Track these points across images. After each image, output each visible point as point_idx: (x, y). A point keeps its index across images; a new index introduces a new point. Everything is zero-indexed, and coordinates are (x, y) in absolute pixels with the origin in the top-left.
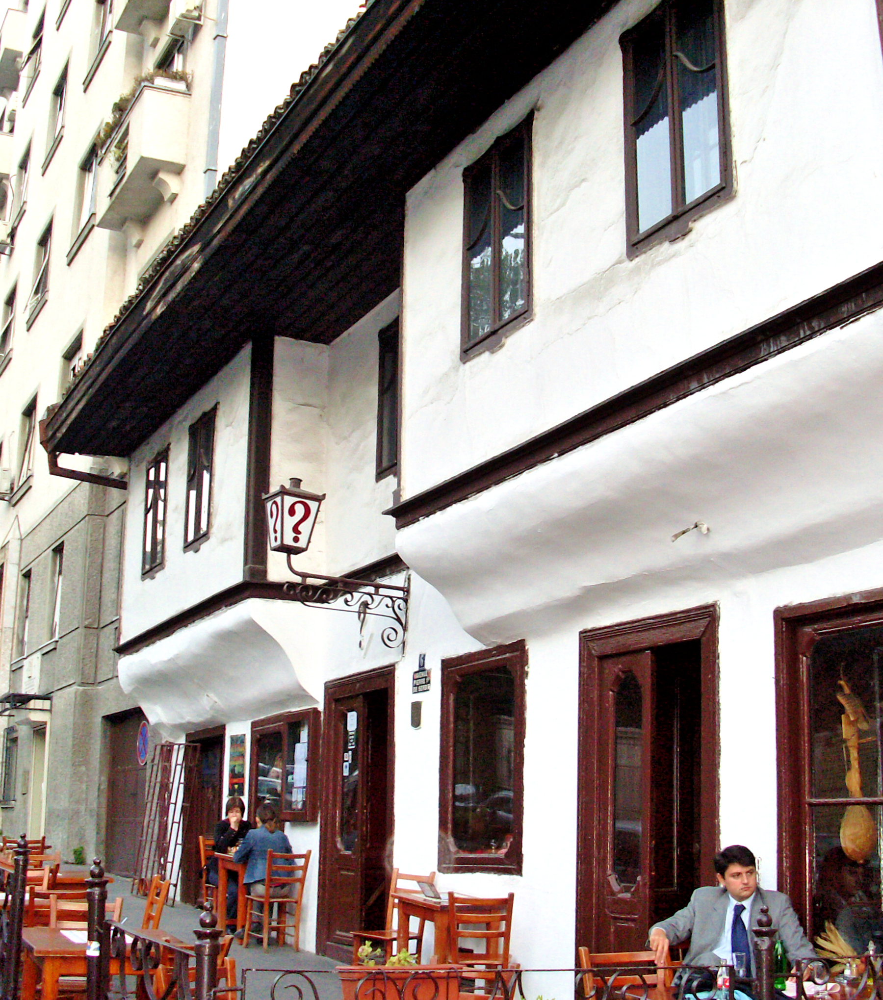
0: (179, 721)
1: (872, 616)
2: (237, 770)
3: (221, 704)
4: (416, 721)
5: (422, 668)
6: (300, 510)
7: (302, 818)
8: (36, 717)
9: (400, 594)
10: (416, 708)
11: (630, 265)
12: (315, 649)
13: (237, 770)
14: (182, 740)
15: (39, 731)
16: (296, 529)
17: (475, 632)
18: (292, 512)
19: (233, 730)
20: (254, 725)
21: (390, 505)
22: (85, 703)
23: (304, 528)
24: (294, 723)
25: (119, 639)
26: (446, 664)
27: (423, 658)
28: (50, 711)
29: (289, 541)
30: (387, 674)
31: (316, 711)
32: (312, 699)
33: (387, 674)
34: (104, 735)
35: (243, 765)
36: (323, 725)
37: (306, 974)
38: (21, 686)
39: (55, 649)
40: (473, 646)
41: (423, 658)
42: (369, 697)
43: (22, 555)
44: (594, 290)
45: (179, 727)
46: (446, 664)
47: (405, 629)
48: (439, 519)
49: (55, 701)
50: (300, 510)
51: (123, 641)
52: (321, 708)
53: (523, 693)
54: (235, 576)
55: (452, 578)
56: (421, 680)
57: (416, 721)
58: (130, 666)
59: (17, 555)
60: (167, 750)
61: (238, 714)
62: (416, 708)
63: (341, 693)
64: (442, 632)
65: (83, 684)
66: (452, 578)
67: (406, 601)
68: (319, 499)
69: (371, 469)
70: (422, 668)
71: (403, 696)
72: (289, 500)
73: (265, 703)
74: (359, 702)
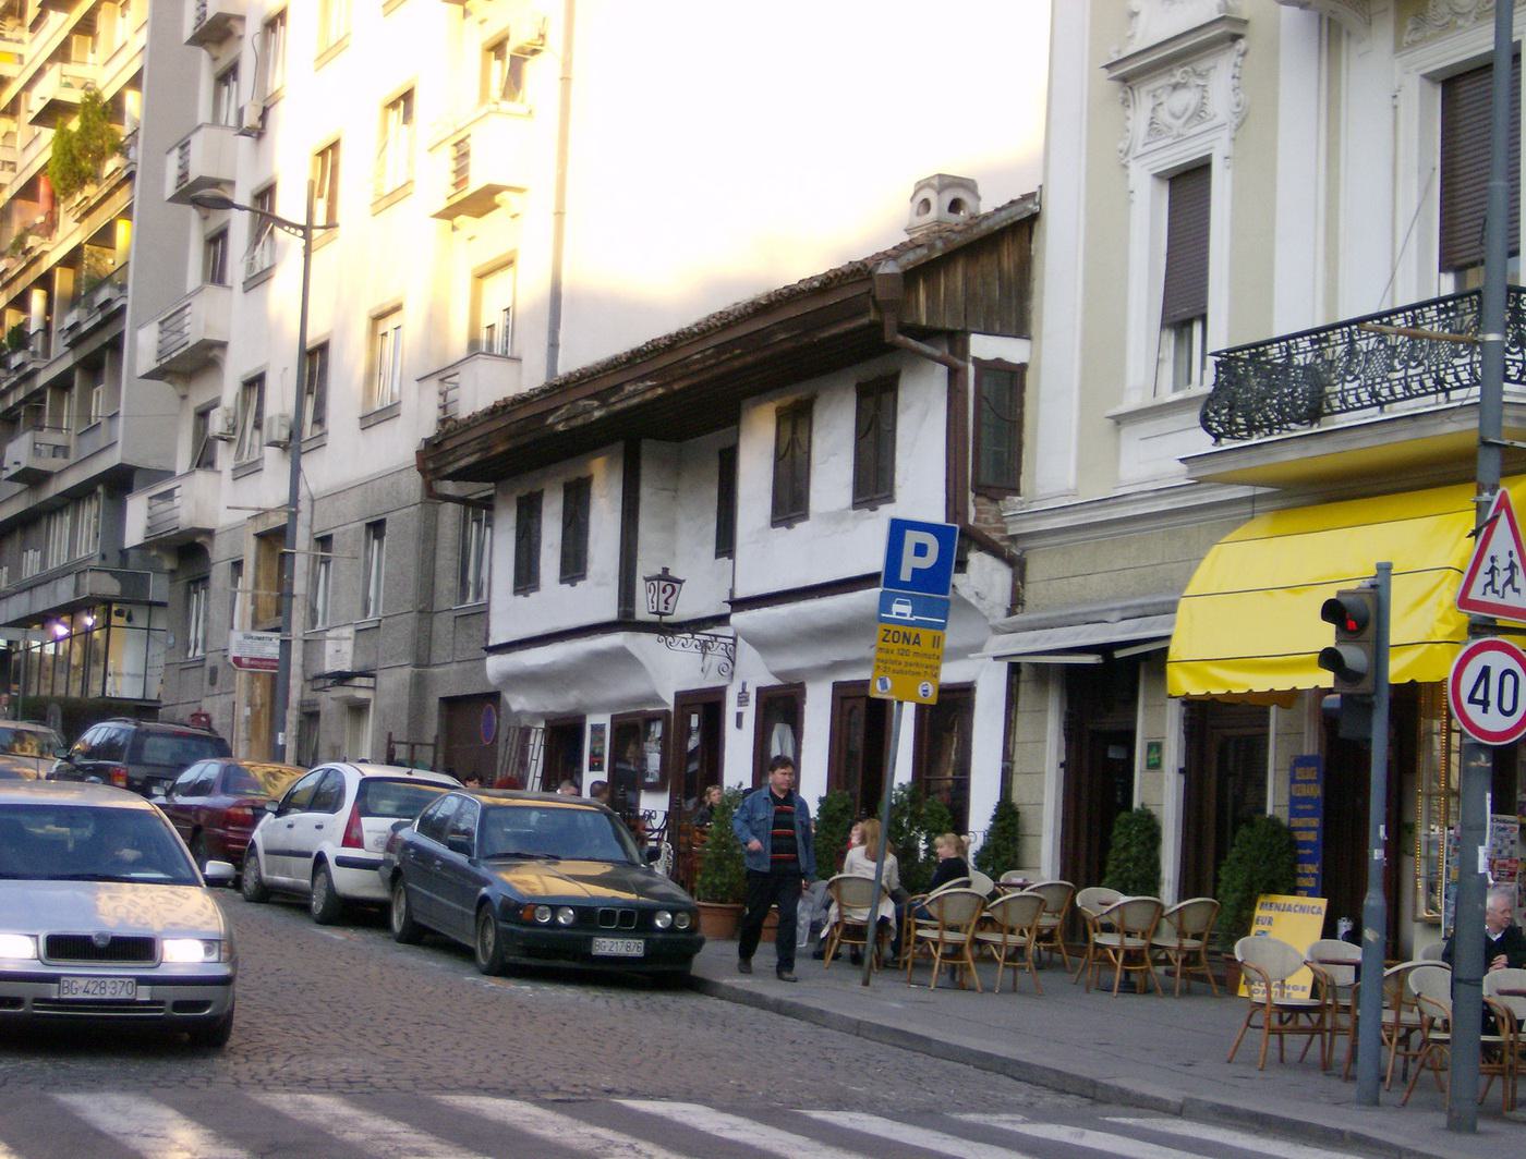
0: (542, 710)
1: (1099, 513)
2: (597, 751)
3: (587, 700)
4: (739, 725)
5: (744, 691)
6: (669, 589)
7: (654, 788)
8: (361, 694)
9: (731, 641)
10: (739, 716)
11: (853, 512)
12: (672, 669)
13: (597, 751)
14: (542, 725)
15: (358, 709)
16: (666, 602)
17: (777, 675)
18: (664, 591)
19: (592, 720)
20: (613, 717)
21: (727, 599)
22: (419, 685)
23: (671, 601)
24: (651, 718)
25: (487, 639)
26: (760, 690)
27: (744, 684)
28: (374, 688)
29: (662, 610)
30: (720, 692)
31: (667, 713)
32: (666, 704)
33: (720, 692)
34: (441, 715)
35: (603, 747)
36: (675, 723)
37: (1503, 518)
38: (323, 664)
39: (378, 627)
40: (775, 682)
41: (744, 684)
42: (707, 706)
43: (315, 517)
44: (836, 517)
45: (542, 715)
46: (760, 690)
47: (733, 663)
48: (756, 613)
49: (379, 679)
50: (669, 589)
51: (491, 643)
52: (671, 708)
53: (802, 713)
54: (610, 613)
55: (763, 644)
56: (743, 699)
57: (739, 725)
58: (495, 665)
59: (309, 516)
60: (526, 733)
61: (599, 708)
62: (739, 716)
63: (686, 700)
64: (756, 672)
65: (417, 666)
66: (763, 644)
67: (734, 645)
68: (680, 582)
69: (711, 548)
70: (744, 691)
71: (731, 708)
72: (663, 583)
73: (623, 703)
74: (701, 709)
